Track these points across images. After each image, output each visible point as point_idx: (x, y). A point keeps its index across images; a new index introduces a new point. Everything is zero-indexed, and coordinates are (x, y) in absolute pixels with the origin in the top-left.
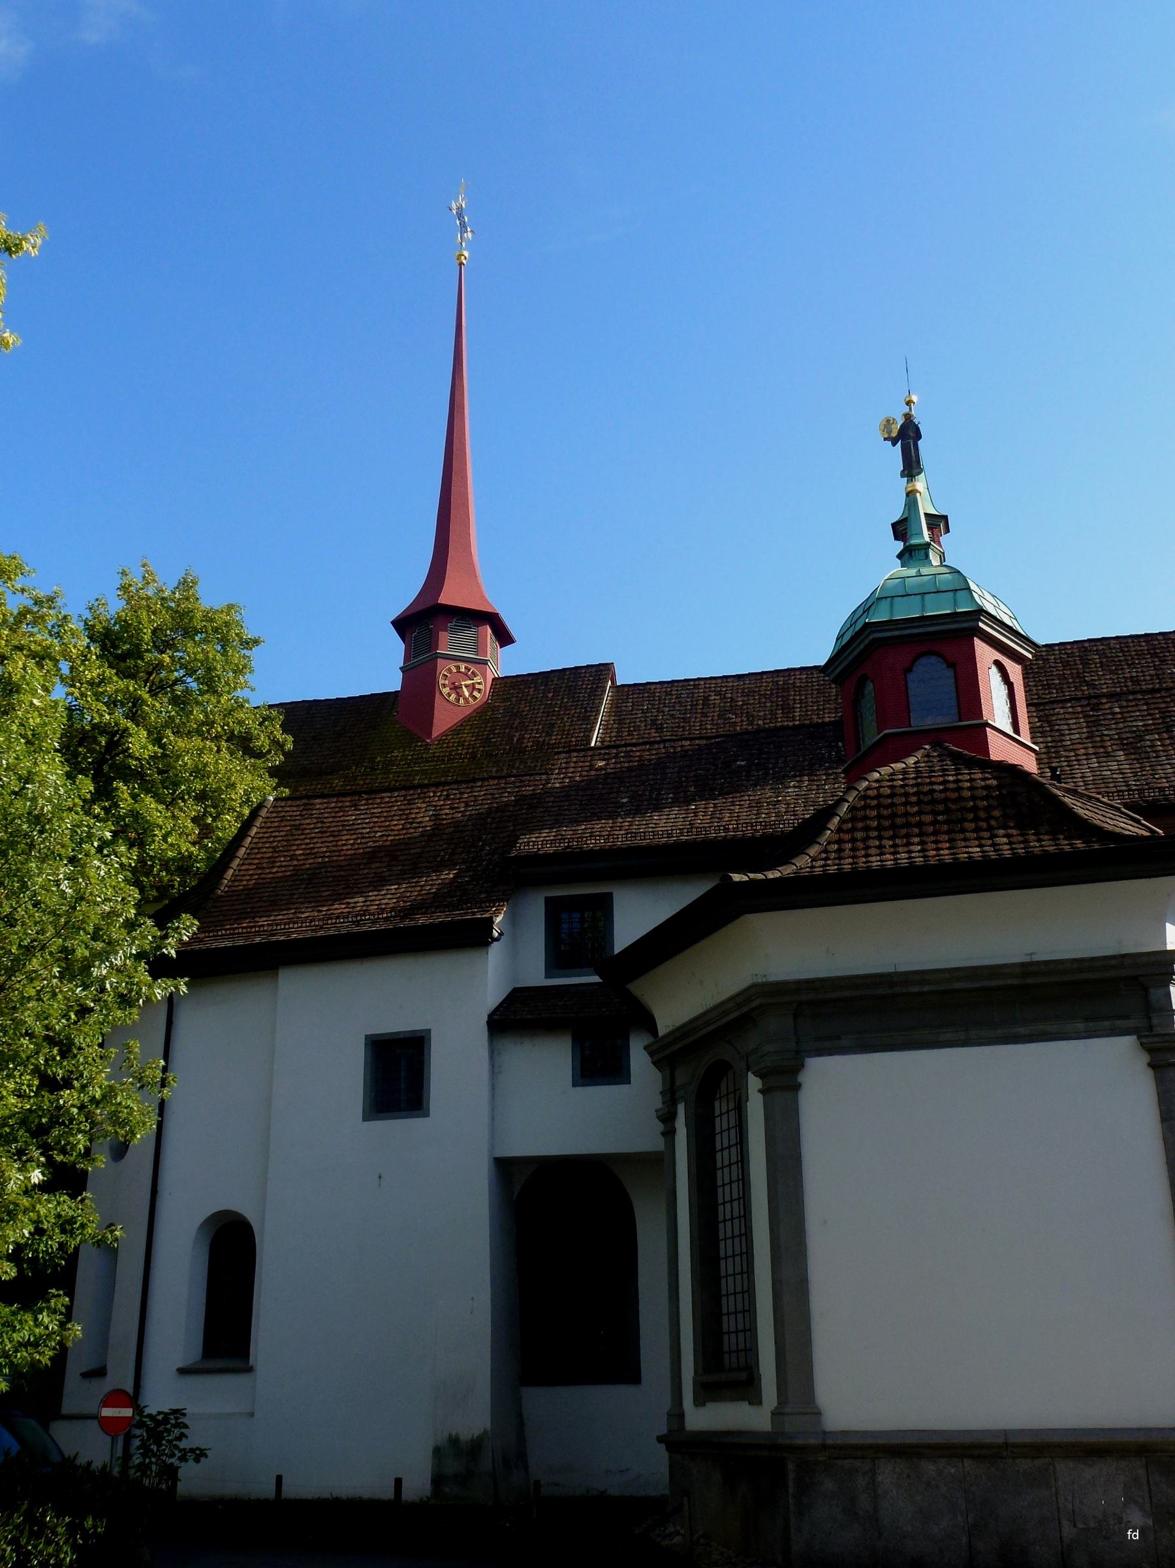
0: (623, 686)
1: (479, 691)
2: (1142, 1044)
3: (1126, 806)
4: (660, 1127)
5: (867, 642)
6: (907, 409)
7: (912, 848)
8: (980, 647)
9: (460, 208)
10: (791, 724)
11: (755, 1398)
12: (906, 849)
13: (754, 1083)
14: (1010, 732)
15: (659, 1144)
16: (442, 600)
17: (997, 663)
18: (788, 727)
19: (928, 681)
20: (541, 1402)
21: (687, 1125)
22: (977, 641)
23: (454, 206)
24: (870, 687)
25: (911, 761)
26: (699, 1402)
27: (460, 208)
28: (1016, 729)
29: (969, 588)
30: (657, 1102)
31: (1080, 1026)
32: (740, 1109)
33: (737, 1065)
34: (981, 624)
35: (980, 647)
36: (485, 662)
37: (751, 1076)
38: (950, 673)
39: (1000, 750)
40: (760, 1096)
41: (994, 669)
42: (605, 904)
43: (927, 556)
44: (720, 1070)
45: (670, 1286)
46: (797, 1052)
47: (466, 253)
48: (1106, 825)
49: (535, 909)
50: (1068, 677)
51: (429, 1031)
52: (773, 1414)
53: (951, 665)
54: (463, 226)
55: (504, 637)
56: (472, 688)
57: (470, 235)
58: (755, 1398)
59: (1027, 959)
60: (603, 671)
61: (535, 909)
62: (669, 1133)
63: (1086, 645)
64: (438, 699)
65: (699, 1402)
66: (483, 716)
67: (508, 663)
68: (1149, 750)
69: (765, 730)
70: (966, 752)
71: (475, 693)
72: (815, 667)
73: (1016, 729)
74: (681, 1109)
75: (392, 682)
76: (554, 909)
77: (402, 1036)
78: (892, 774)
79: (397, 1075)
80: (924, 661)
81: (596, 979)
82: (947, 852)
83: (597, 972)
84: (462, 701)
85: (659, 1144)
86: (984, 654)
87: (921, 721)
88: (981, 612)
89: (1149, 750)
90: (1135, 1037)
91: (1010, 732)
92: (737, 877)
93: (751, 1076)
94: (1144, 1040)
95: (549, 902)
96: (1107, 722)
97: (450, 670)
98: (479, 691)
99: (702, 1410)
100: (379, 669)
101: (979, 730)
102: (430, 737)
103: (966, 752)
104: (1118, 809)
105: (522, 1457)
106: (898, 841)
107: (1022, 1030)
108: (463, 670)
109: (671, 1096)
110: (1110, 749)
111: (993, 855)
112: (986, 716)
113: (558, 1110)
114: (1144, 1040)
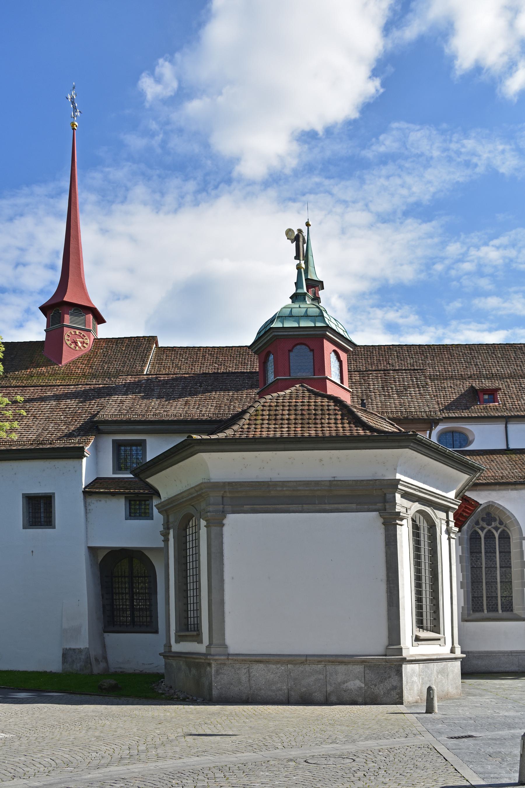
0: (162, 347)
1: (87, 344)
2: (381, 516)
3: (389, 418)
4: (162, 538)
5: (271, 336)
6: (304, 229)
7: (283, 429)
8: (326, 343)
9: (72, 98)
10: (245, 371)
11: (200, 642)
12: (280, 430)
13: (203, 523)
14: (339, 383)
15: (162, 545)
16: (66, 299)
17: (335, 351)
18: (244, 373)
19: (300, 358)
20: (111, 638)
21: (174, 538)
22: (325, 341)
23: (69, 97)
24: (271, 357)
25: (288, 391)
26: (177, 641)
27: (72, 98)
28: (342, 382)
29: (323, 316)
30: (161, 528)
31: (354, 506)
32: (197, 532)
33: (189, 514)
34: (327, 333)
35: (326, 343)
36: (89, 331)
37: (201, 520)
38: (312, 353)
39: (332, 390)
40: (205, 528)
41: (333, 354)
42: (142, 444)
43: (305, 299)
44: (188, 518)
45: (166, 599)
46: (223, 512)
47: (76, 123)
48: (377, 426)
49: (107, 443)
50: (367, 361)
51: (54, 493)
52: (207, 647)
53: (312, 350)
54: (75, 108)
55: (100, 320)
56: (83, 343)
57: (79, 114)
58: (200, 642)
59: (333, 479)
60: (153, 339)
61: (107, 443)
62: (166, 541)
63: (391, 347)
64: (65, 347)
65: (177, 641)
66: (88, 357)
67: (103, 332)
68: (408, 395)
69: (232, 373)
70: (315, 390)
71: (85, 345)
72: (246, 346)
73: (342, 382)
74: (171, 532)
75: (42, 337)
76: (117, 445)
77: (40, 495)
78: (278, 397)
79: (39, 510)
80: (298, 347)
81: (131, 476)
82: (300, 432)
83: (131, 473)
84: (77, 348)
85: (162, 545)
86: (328, 347)
87: (294, 375)
88: (328, 327)
89: (408, 395)
90: (378, 513)
91: (339, 383)
92: (195, 436)
93: (201, 520)
94: (382, 514)
95: (114, 441)
96: (391, 382)
97: (71, 333)
98: (87, 344)
99: (178, 645)
100: (35, 331)
101: (323, 381)
102: (61, 364)
103: (315, 390)
104: (385, 420)
105: (105, 658)
106: (277, 426)
107: (327, 507)
108: (77, 333)
109: (167, 527)
110: (391, 393)
111: (320, 435)
112: (327, 374)
113: (119, 529)
114: (382, 514)
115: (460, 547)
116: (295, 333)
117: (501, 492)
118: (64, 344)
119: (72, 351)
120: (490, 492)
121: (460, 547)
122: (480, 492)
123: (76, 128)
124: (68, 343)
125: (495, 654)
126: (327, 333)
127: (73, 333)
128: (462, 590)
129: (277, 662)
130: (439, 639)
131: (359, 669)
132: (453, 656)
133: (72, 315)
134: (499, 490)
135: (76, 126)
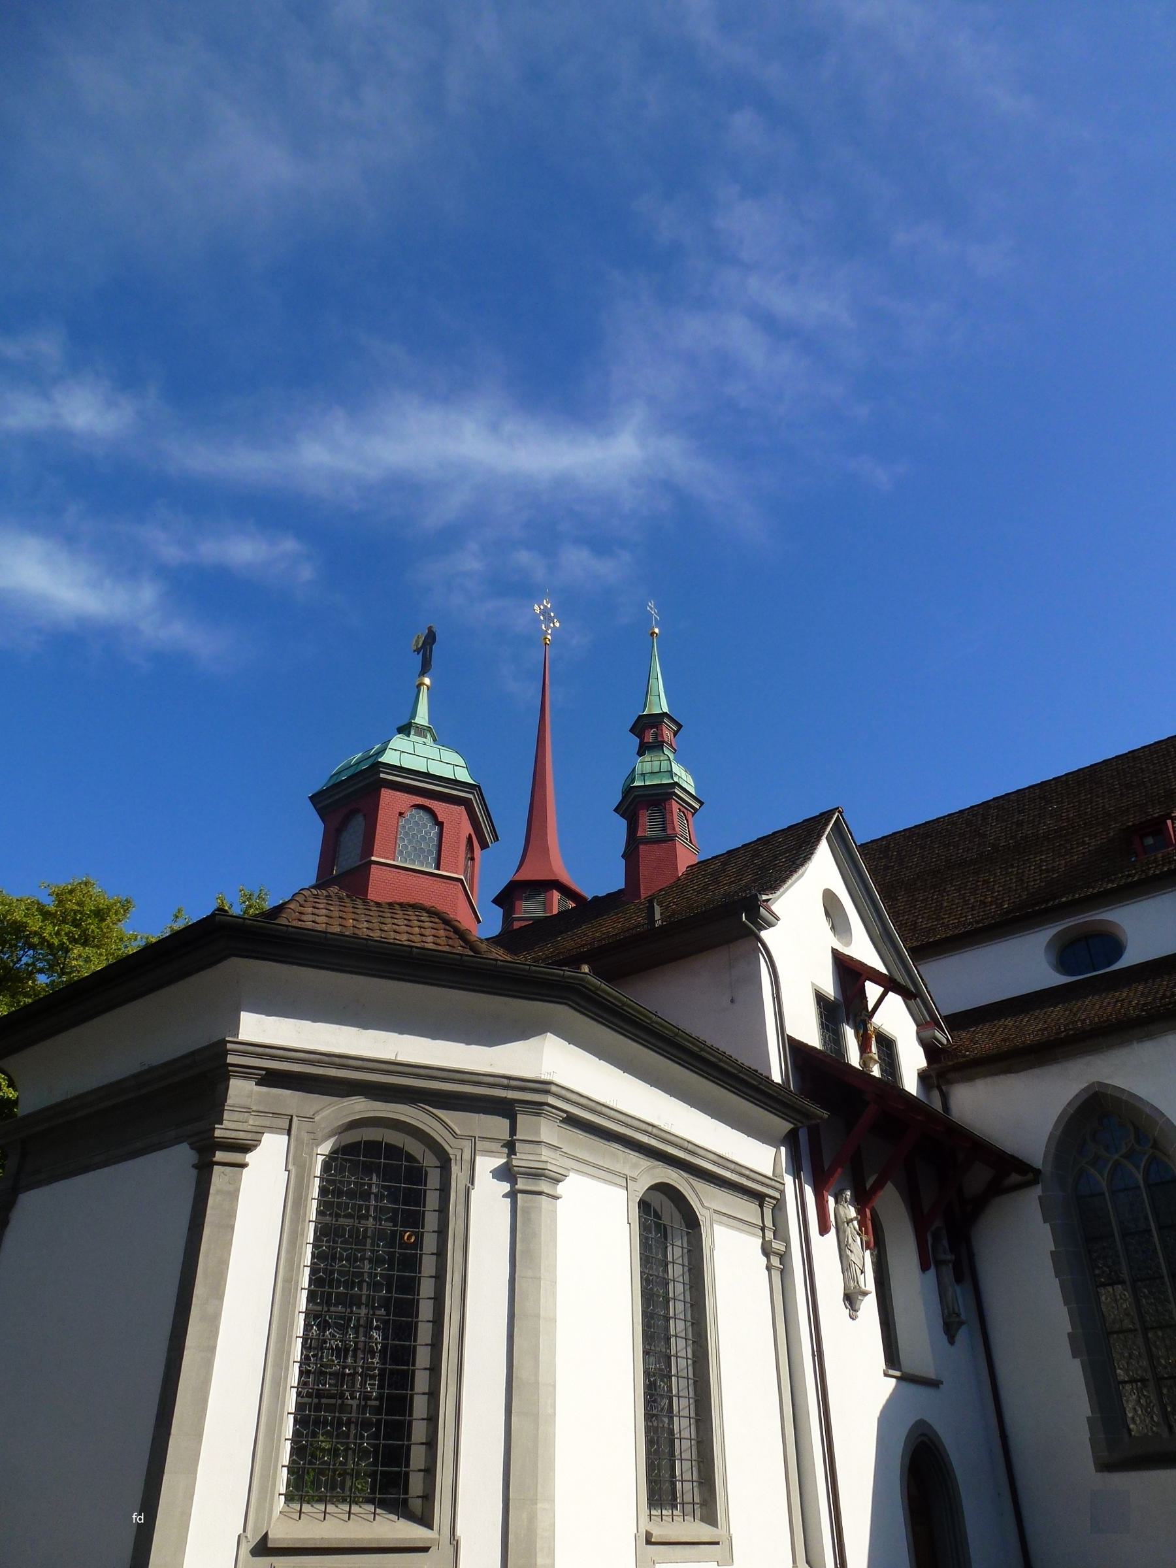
34: (382, 775)
126: (382, 775)
133: (527, 899)
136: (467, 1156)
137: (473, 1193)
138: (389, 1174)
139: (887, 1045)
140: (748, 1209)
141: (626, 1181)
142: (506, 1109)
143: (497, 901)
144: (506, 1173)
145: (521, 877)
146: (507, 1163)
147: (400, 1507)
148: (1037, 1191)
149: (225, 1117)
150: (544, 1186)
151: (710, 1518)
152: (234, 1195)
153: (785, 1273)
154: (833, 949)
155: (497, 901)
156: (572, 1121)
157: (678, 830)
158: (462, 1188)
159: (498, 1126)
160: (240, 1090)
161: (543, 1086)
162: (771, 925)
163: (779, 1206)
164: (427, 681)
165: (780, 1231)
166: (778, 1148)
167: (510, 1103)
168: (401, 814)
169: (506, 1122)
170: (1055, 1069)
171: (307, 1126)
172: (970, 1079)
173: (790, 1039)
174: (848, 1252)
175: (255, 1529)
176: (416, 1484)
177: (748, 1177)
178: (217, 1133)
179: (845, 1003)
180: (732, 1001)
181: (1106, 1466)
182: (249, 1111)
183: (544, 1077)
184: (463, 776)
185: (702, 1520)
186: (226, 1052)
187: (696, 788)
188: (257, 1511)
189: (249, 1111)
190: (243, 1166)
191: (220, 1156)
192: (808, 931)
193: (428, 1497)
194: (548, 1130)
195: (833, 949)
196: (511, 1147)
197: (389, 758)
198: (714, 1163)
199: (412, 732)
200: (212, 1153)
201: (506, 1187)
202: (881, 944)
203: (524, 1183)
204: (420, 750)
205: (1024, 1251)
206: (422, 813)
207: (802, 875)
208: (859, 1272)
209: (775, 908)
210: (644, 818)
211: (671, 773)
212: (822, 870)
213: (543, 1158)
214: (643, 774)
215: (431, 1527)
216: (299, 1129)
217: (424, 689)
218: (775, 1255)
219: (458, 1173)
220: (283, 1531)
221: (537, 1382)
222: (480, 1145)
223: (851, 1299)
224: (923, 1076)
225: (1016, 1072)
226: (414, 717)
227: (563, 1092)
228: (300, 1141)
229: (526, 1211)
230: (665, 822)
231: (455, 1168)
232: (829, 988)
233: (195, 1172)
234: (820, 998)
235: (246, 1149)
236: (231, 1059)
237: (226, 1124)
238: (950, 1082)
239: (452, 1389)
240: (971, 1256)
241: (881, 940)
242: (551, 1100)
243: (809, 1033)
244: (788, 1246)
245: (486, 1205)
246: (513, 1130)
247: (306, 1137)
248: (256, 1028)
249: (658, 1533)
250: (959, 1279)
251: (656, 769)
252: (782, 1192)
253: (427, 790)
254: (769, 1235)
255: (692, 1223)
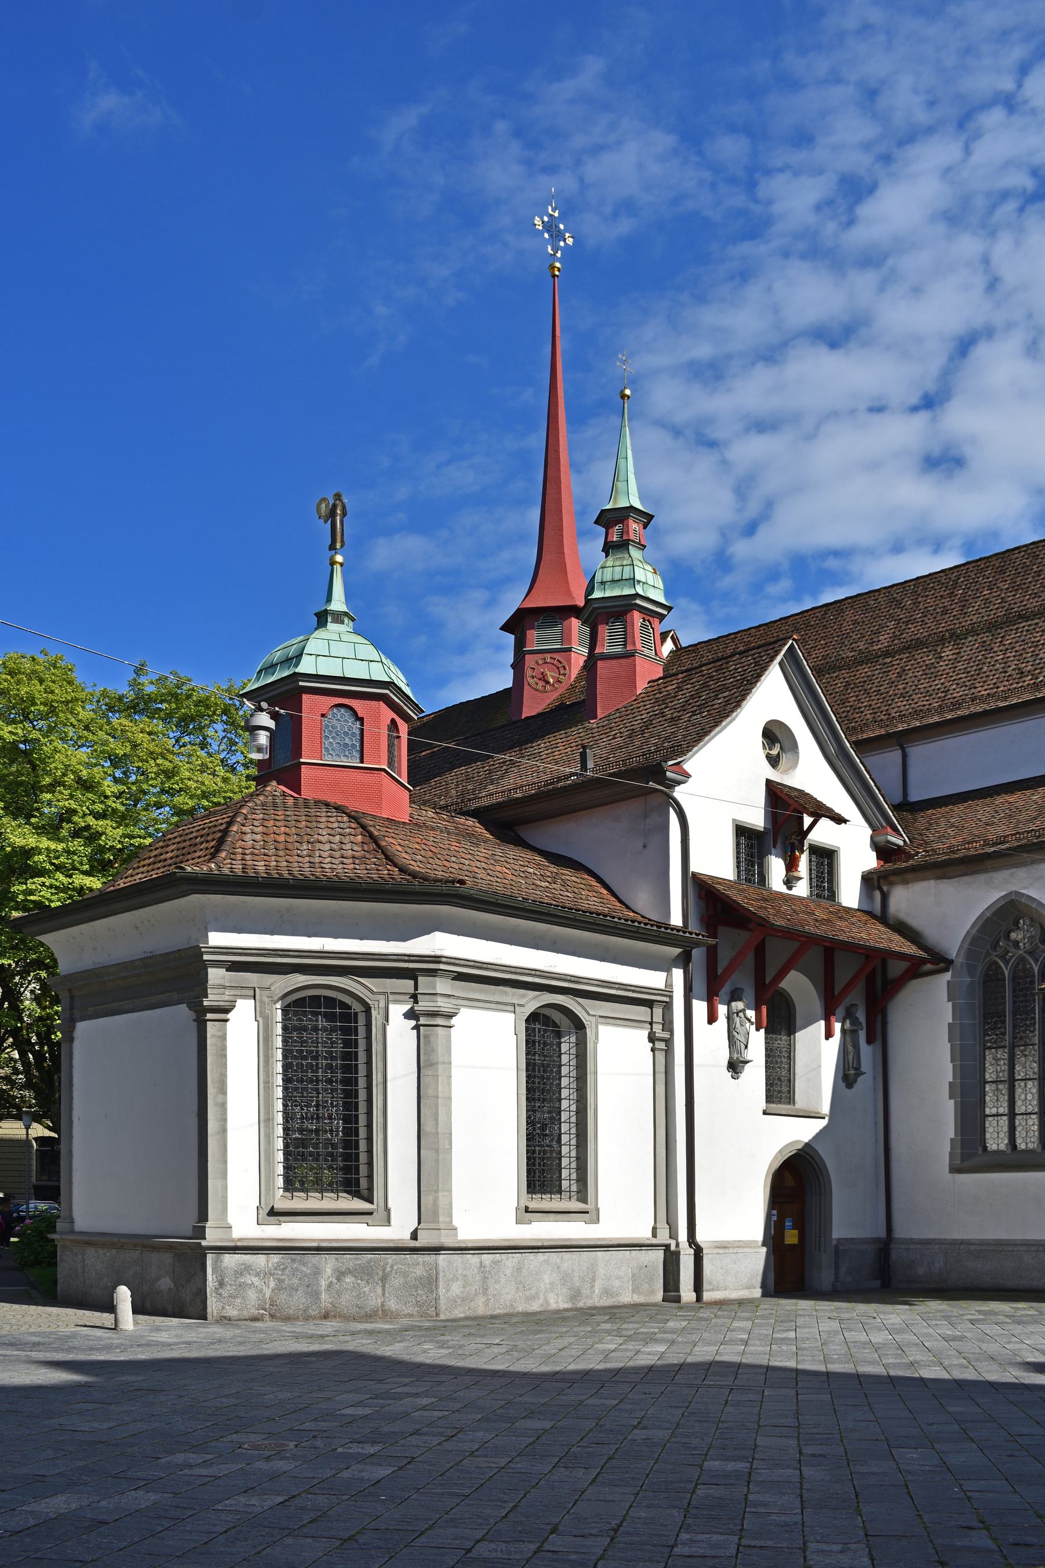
34: (301, 683)
115: (950, 1003)
116: (281, 690)
117: (1036, 866)
118: (526, 687)
119: (539, 694)
120: (1013, 870)
121: (950, 1003)
122: (993, 874)
123: (557, 273)
124: (531, 681)
125: (1010, 1248)
126: (301, 683)
127: (540, 662)
128: (952, 1102)
129: (103, 1246)
130: (371, 1214)
131: (168, 1258)
132: (655, 1241)
133: (539, 627)
134: (1033, 862)
135: (559, 270)
136: (382, 1004)
137: (388, 1028)
138: (330, 1017)
139: (826, 859)
140: (641, 1013)
141: (513, 1007)
142: (411, 975)
143: (507, 627)
144: (410, 1015)
145: (529, 605)
146: (412, 1008)
147: (357, 1194)
148: (948, 976)
149: (209, 991)
150: (439, 1021)
151: (582, 1195)
152: (223, 1038)
153: (669, 1052)
154: (767, 780)
155: (507, 627)
156: (460, 977)
157: (639, 646)
158: (380, 1024)
159: (407, 985)
160: (215, 975)
161: (436, 959)
162: (679, 783)
163: (668, 1007)
164: (339, 558)
165: (668, 1024)
166: (668, 970)
167: (412, 971)
168: (323, 715)
169: (412, 982)
170: (982, 878)
171: (266, 993)
172: (906, 882)
173: (694, 875)
174: (735, 1033)
175: (266, 1204)
176: (363, 1183)
177: (633, 991)
178: (205, 1003)
179: (787, 816)
180: (644, 846)
181: (950, 1172)
182: (225, 987)
183: (438, 953)
184: (378, 673)
185: (578, 1200)
186: (202, 954)
187: (667, 595)
188: (266, 1196)
189: (225, 987)
190: (227, 1021)
191: (209, 1016)
192: (720, 786)
193: (370, 1189)
194: (442, 985)
195: (767, 780)
196: (415, 997)
197: (306, 666)
198: (598, 986)
199: (329, 619)
200: (204, 1015)
201: (413, 1023)
202: (839, 764)
203: (427, 1021)
204: (338, 649)
205: (929, 1023)
206: (342, 710)
207: (734, 719)
208: (743, 1047)
209: (687, 767)
210: (604, 631)
211: (633, 581)
212: (772, 697)
213: (439, 1004)
214: (603, 583)
215: (372, 1203)
216: (261, 995)
217: (338, 569)
218: (660, 1043)
219: (376, 1016)
220: (281, 1205)
221: (437, 1133)
222: (391, 997)
223: (735, 1066)
224: (869, 880)
225: (950, 878)
226: (329, 599)
227: (453, 961)
228: (262, 1003)
229: (426, 1037)
230: (626, 637)
231: (374, 1013)
232: (757, 819)
233: (195, 1023)
234: (742, 831)
235: (227, 1011)
236: (205, 957)
237: (211, 997)
238: (892, 884)
239: (381, 1136)
240: (885, 1024)
241: (838, 761)
242: (442, 967)
243: (716, 859)
244: (672, 1034)
245: (398, 1037)
246: (416, 988)
247: (266, 1000)
248: (217, 939)
249: (533, 1205)
250: (870, 1041)
251: (617, 577)
252: (671, 997)
253: (346, 692)
254: (658, 1029)
255: (579, 1026)
